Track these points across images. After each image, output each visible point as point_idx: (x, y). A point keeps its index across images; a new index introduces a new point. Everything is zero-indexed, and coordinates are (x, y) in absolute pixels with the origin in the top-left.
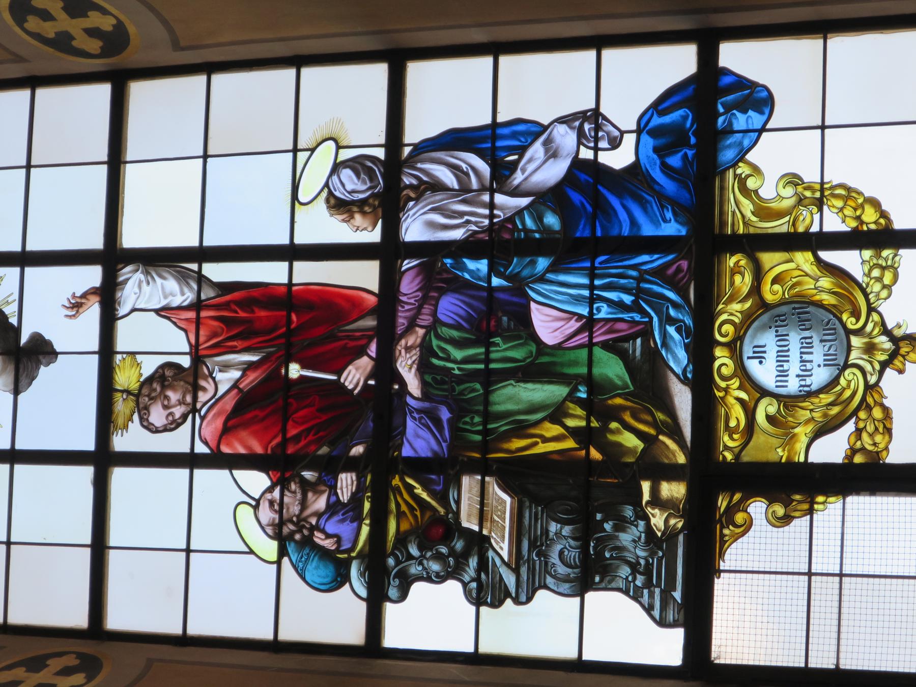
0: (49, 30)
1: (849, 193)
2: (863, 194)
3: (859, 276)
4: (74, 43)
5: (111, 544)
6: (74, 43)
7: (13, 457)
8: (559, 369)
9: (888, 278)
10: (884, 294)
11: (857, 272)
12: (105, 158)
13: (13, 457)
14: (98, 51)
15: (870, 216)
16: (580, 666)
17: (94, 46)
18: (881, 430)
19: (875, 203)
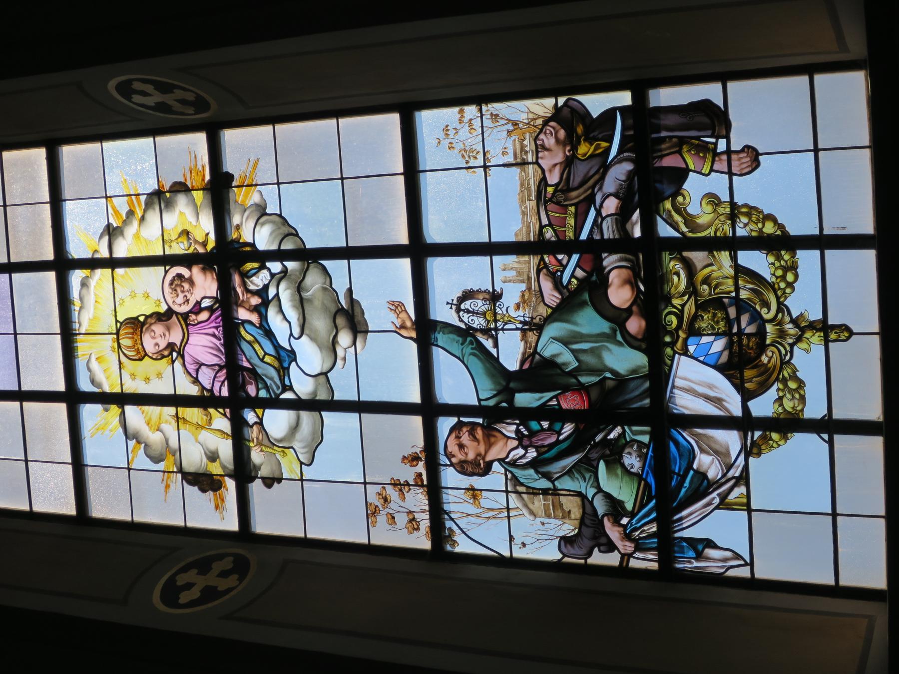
0: (218, 567)
1: (751, 211)
2: (762, 212)
3: (768, 277)
4: (195, 571)
5: (340, 120)
6: (195, 571)
7: (10, 268)
8: (724, 403)
9: (790, 277)
10: (788, 291)
11: (766, 272)
12: (373, 542)
13: (10, 268)
14: (178, 578)
15: (769, 228)
16: (31, 516)
17: (181, 580)
18: (176, 337)
19: (774, 220)
